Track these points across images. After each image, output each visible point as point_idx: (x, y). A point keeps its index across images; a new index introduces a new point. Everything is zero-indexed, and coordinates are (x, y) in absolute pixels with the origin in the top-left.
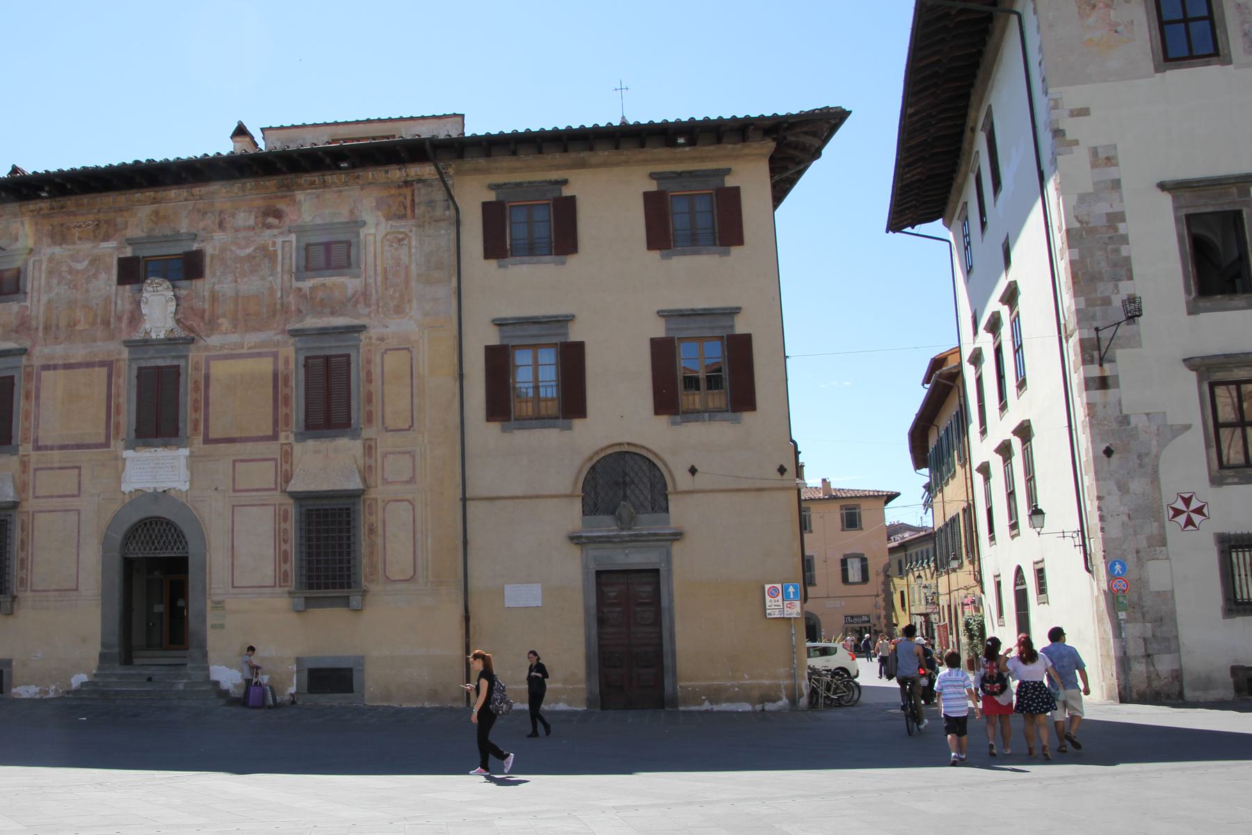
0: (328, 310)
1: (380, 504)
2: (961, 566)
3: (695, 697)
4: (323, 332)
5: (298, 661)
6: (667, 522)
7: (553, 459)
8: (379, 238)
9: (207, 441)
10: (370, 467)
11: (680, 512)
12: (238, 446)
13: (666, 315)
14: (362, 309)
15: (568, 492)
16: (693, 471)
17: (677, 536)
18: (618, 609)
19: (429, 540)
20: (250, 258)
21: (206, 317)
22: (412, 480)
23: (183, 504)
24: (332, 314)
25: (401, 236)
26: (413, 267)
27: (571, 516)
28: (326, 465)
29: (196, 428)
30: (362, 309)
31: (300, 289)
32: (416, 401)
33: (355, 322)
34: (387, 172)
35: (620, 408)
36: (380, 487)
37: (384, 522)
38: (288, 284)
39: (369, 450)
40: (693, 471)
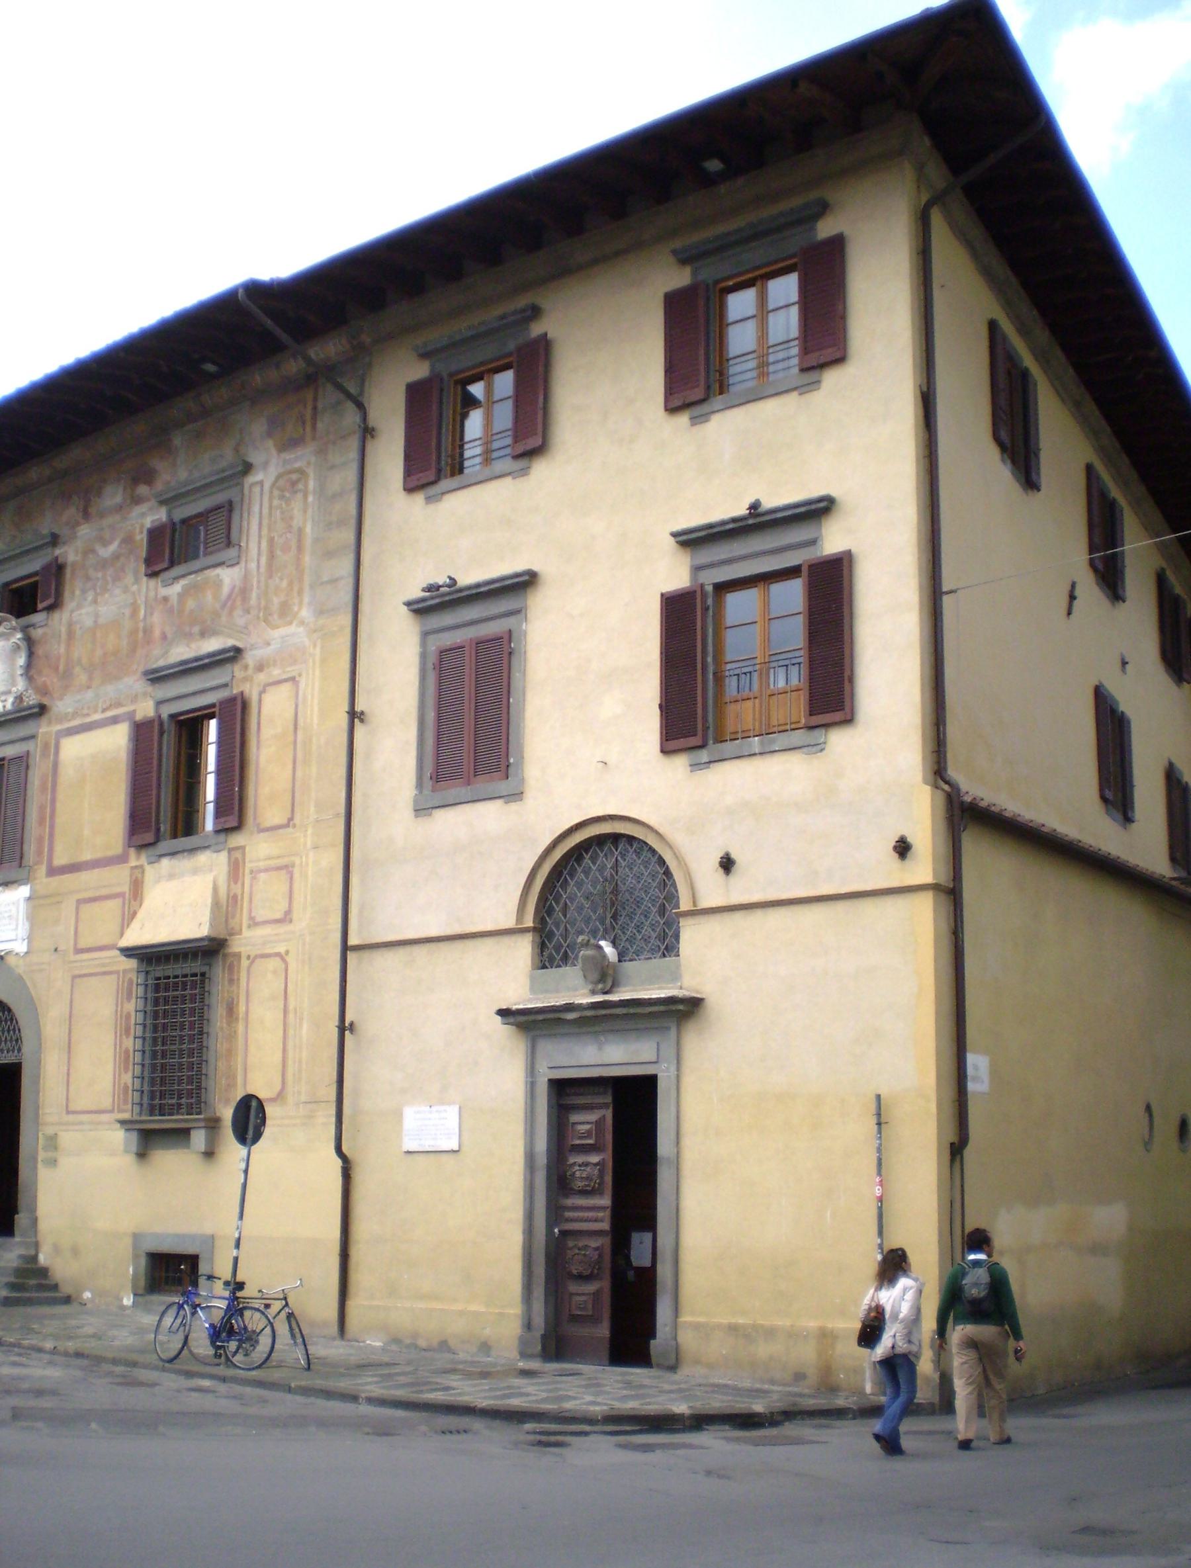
0: (196, 629)
1: (245, 963)
2: (824, 339)
3: (718, 1348)
4: (188, 669)
5: (137, 1237)
6: (675, 976)
7: (489, 855)
8: (267, 486)
9: (53, 871)
10: (235, 897)
11: (705, 959)
12: (85, 877)
13: (692, 540)
14: (240, 619)
15: (510, 923)
16: (727, 864)
17: (684, 1010)
18: (594, 1159)
19: (305, 1026)
20: (116, 557)
21: (61, 668)
22: (287, 918)
23: (20, 978)
24: (203, 634)
25: (294, 477)
26: (308, 529)
27: (511, 974)
28: (176, 901)
29: (40, 853)
30: (240, 619)
31: (166, 599)
32: (299, 774)
33: (212, 645)
34: (278, 366)
35: (591, 739)
36: (246, 933)
37: (247, 991)
38: (152, 594)
39: (235, 870)
40: (727, 864)
